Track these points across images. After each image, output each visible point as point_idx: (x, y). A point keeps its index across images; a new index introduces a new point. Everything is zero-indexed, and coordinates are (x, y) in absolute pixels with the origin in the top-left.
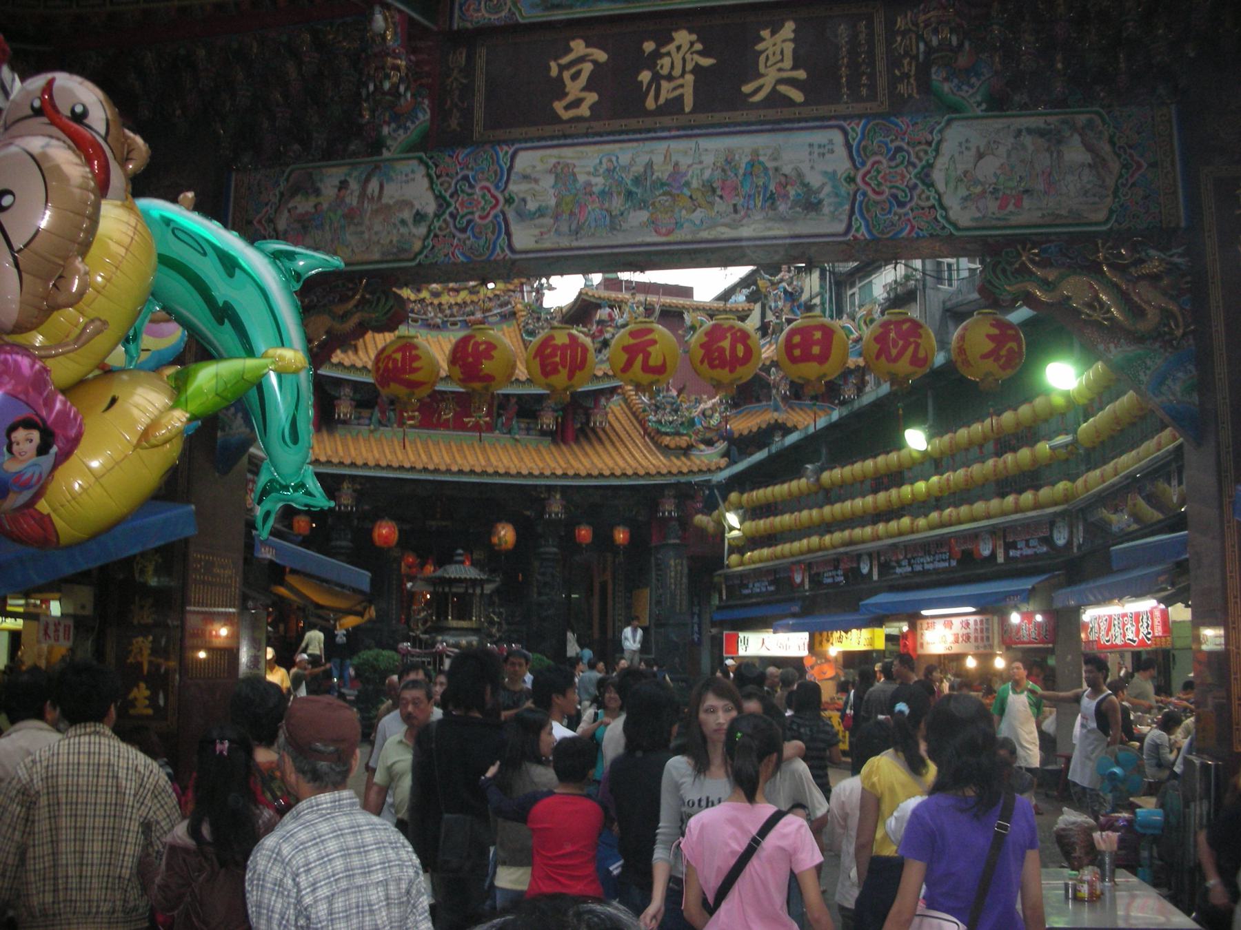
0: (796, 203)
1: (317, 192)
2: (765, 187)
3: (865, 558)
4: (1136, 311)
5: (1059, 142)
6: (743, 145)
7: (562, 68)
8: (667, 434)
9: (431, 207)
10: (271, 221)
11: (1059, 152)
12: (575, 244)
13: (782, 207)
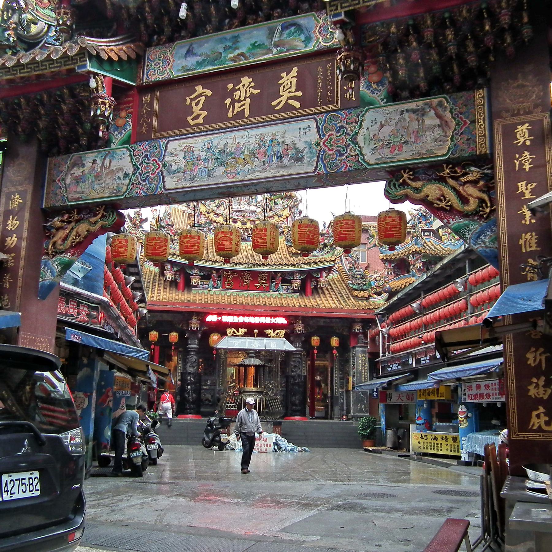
0: (292, 158)
1: (83, 165)
2: (278, 151)
4: (464, 200)
5: (423, 115)
6: (268, 131)
7: (192, 100)
8: (357, 290)
9: (131, 171)
10: (63, 180)
11: (422, 120)
12: (192, 185)
13: (285, 161)
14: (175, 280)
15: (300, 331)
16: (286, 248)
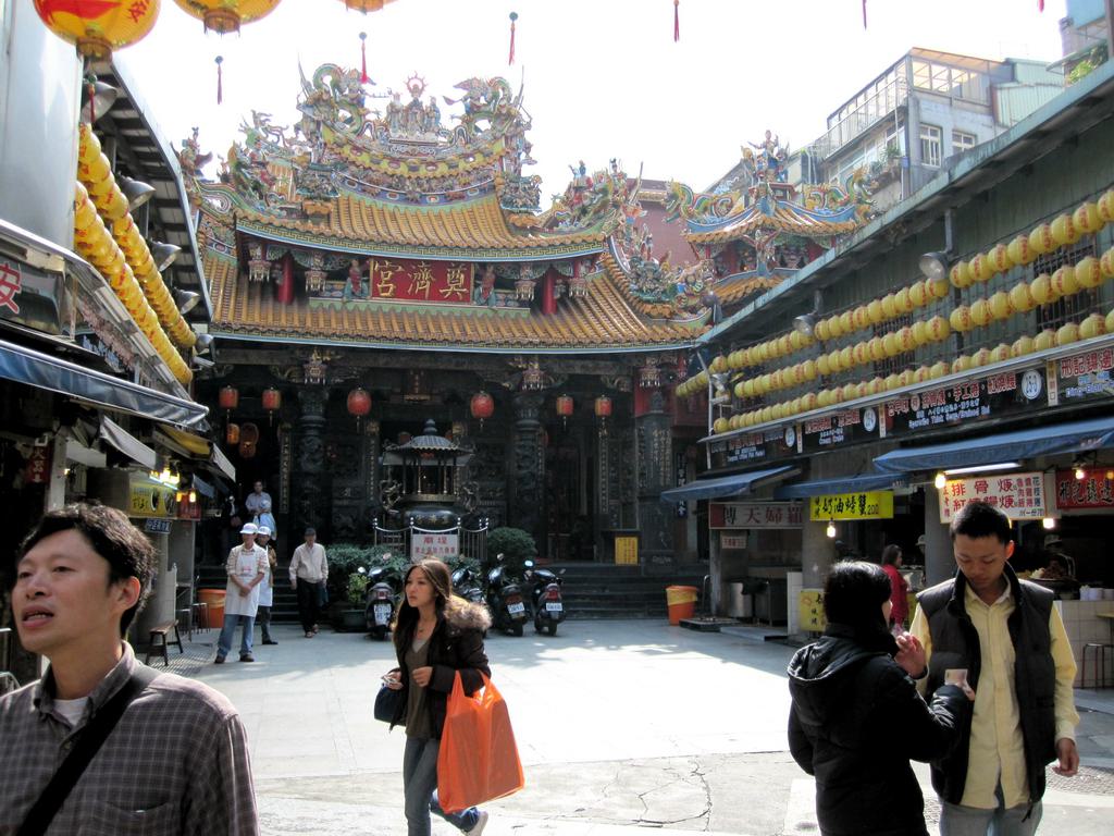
3: (790, 430)
8: (648, 302)
14: (273, 280)
15: (259, 275)
16: (501, 219)
